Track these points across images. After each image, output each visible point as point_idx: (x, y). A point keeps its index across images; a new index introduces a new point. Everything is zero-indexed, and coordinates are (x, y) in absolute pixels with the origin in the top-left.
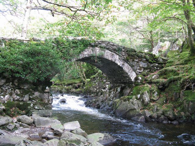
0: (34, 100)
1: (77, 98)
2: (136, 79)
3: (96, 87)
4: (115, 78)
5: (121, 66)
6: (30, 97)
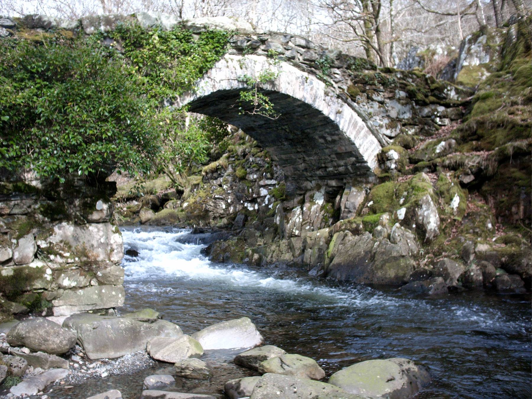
0: (56, 254)
1: (169, 237)
4: (304, 161)
5: (332, 117)
6: (39, 243)
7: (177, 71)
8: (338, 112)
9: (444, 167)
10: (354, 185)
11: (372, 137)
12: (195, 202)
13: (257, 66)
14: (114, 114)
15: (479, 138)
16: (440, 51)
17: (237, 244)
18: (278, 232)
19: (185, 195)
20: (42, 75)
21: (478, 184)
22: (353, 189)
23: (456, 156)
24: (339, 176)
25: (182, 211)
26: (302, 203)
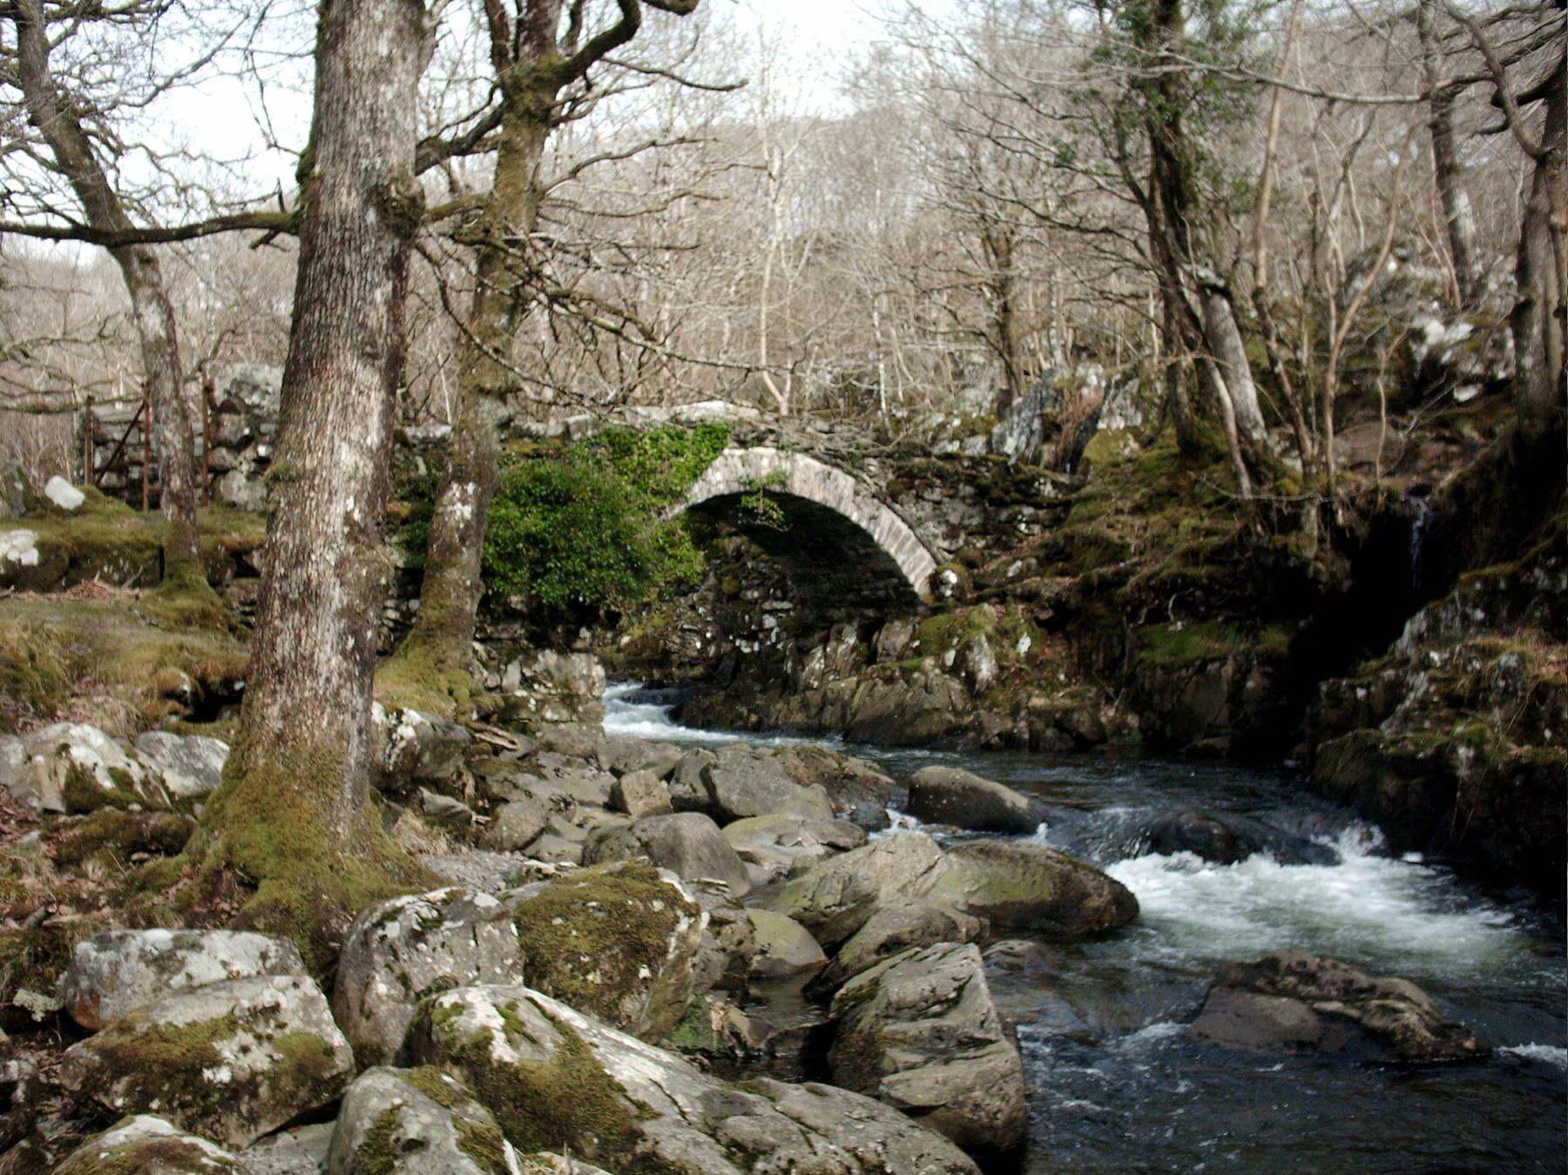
2: (936, 581)
3: (701, 633)
5: (864, 524)
7: (668, 476)
8: (873, 518)
9: (1015, 596)
10: (898, 618)
11: (922, 551)
12: (645, 636)
13: (765, 460)
14: (616, 539)
15: (1067, 558)
16: (1093, 380)
17: (724, 703)
18: (789, 685)
19: (624, 621)
20: (545, 499)
21: (1058, 621)
22: (897, 624)
23: (1032, 582)
24: (878, 604)
25: (619, 650)
26: (825, 641)
